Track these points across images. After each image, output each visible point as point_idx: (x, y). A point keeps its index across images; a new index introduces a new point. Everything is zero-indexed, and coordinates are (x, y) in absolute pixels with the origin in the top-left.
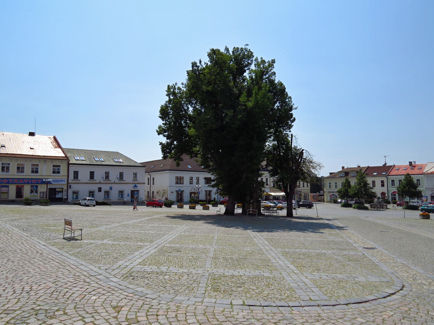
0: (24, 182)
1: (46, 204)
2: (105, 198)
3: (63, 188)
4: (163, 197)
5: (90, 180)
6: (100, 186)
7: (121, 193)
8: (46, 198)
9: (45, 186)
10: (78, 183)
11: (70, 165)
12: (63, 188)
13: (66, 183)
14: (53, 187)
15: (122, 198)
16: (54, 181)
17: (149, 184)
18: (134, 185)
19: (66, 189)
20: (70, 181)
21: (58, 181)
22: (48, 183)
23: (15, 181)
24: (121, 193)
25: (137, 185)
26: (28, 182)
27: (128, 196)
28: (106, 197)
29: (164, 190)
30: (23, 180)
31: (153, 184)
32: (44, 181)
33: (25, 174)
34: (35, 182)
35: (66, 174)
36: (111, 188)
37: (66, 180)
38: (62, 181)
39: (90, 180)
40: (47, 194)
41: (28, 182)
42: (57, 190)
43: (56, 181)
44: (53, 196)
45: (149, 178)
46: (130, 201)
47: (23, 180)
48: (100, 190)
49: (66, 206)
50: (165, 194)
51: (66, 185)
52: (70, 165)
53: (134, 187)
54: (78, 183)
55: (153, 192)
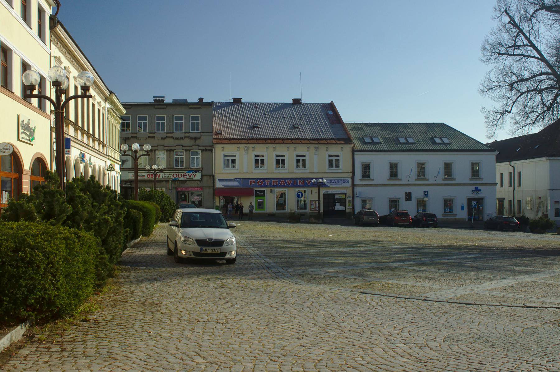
0: (286, 183)
1: (317, 221)
2: (445, 212)
3: (346, 194)
4: (537, 211)
5: (472, 178)
6: (408, 189)
7: (448, 203)
8: (318, 212)
9: (316, 190)
10: (371, 185)
11: (356, 153)
12: (346, 194)
13: (349, 184)
14: (330, 192)
15: (450, 212)
16: (331, 182)
17: (510, 186)
18: (473, 188)
19: (351, 195)
20: (357, 182)
21: (338, 181)
22: (320, 185)
23: (274, 183)
24: (448, 203)
25: (480, 187)
26: (292, 184)
27: (463, 208)
28: (447, 210)
29: (540, 198)
30: (285, 181)
31: (520, 185)
32: (320, 183)
33: (287, 171)
34: (303, 183)
35: (351, 170)
36: (426, 194)
37: (350, 180)
38: (344, 181)
39: (472, 178)
40: (319, 203)
41: (292, 184)
42: (337, 197)
43: (335, 181)
44: (330, 208)
45: (510, 173)
46: (467, 220)
47: (285, 181)
48: (409, 197)
49: (446, 229)
50: (541, 206)
51: (351, 188)
52: (356, 153)
53: (473, 191)
54: (371, 185)
55: (519, 201)
